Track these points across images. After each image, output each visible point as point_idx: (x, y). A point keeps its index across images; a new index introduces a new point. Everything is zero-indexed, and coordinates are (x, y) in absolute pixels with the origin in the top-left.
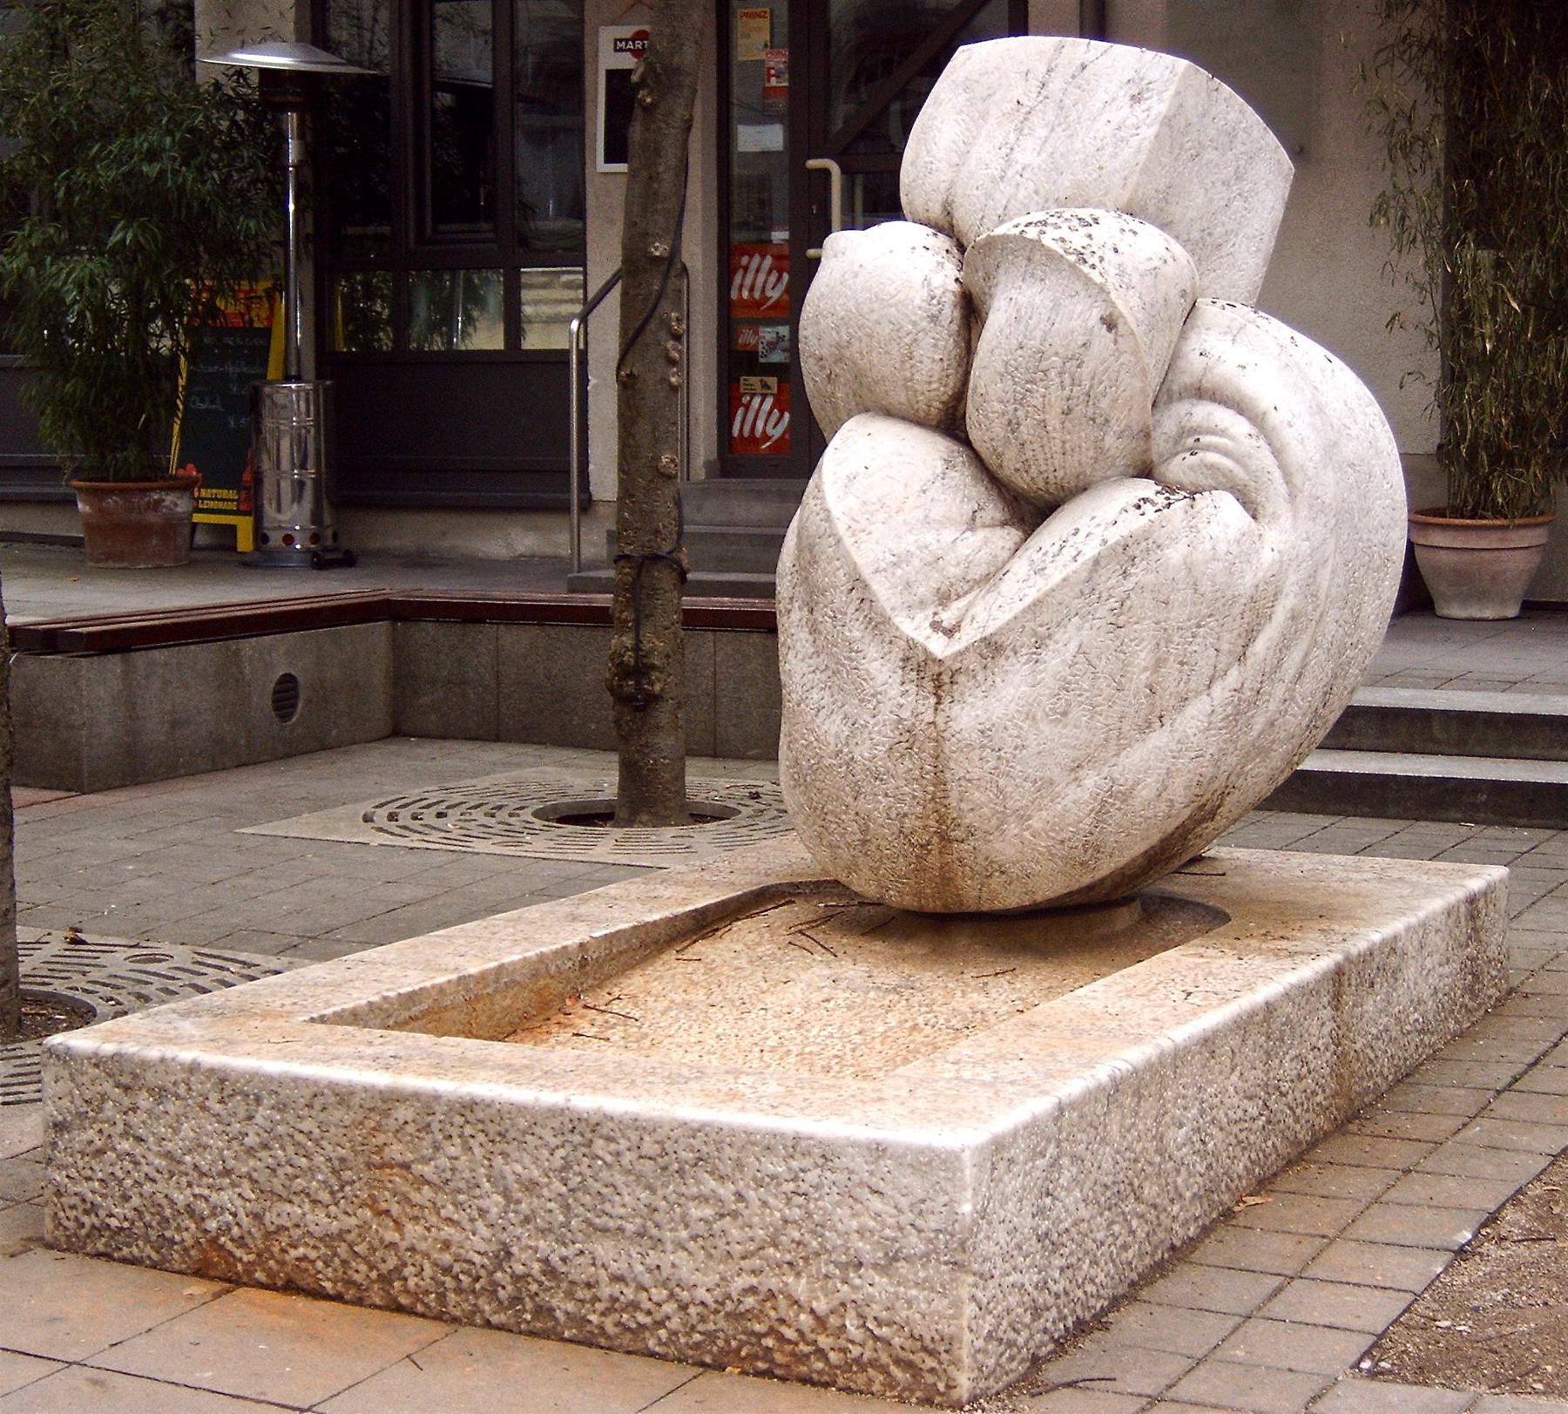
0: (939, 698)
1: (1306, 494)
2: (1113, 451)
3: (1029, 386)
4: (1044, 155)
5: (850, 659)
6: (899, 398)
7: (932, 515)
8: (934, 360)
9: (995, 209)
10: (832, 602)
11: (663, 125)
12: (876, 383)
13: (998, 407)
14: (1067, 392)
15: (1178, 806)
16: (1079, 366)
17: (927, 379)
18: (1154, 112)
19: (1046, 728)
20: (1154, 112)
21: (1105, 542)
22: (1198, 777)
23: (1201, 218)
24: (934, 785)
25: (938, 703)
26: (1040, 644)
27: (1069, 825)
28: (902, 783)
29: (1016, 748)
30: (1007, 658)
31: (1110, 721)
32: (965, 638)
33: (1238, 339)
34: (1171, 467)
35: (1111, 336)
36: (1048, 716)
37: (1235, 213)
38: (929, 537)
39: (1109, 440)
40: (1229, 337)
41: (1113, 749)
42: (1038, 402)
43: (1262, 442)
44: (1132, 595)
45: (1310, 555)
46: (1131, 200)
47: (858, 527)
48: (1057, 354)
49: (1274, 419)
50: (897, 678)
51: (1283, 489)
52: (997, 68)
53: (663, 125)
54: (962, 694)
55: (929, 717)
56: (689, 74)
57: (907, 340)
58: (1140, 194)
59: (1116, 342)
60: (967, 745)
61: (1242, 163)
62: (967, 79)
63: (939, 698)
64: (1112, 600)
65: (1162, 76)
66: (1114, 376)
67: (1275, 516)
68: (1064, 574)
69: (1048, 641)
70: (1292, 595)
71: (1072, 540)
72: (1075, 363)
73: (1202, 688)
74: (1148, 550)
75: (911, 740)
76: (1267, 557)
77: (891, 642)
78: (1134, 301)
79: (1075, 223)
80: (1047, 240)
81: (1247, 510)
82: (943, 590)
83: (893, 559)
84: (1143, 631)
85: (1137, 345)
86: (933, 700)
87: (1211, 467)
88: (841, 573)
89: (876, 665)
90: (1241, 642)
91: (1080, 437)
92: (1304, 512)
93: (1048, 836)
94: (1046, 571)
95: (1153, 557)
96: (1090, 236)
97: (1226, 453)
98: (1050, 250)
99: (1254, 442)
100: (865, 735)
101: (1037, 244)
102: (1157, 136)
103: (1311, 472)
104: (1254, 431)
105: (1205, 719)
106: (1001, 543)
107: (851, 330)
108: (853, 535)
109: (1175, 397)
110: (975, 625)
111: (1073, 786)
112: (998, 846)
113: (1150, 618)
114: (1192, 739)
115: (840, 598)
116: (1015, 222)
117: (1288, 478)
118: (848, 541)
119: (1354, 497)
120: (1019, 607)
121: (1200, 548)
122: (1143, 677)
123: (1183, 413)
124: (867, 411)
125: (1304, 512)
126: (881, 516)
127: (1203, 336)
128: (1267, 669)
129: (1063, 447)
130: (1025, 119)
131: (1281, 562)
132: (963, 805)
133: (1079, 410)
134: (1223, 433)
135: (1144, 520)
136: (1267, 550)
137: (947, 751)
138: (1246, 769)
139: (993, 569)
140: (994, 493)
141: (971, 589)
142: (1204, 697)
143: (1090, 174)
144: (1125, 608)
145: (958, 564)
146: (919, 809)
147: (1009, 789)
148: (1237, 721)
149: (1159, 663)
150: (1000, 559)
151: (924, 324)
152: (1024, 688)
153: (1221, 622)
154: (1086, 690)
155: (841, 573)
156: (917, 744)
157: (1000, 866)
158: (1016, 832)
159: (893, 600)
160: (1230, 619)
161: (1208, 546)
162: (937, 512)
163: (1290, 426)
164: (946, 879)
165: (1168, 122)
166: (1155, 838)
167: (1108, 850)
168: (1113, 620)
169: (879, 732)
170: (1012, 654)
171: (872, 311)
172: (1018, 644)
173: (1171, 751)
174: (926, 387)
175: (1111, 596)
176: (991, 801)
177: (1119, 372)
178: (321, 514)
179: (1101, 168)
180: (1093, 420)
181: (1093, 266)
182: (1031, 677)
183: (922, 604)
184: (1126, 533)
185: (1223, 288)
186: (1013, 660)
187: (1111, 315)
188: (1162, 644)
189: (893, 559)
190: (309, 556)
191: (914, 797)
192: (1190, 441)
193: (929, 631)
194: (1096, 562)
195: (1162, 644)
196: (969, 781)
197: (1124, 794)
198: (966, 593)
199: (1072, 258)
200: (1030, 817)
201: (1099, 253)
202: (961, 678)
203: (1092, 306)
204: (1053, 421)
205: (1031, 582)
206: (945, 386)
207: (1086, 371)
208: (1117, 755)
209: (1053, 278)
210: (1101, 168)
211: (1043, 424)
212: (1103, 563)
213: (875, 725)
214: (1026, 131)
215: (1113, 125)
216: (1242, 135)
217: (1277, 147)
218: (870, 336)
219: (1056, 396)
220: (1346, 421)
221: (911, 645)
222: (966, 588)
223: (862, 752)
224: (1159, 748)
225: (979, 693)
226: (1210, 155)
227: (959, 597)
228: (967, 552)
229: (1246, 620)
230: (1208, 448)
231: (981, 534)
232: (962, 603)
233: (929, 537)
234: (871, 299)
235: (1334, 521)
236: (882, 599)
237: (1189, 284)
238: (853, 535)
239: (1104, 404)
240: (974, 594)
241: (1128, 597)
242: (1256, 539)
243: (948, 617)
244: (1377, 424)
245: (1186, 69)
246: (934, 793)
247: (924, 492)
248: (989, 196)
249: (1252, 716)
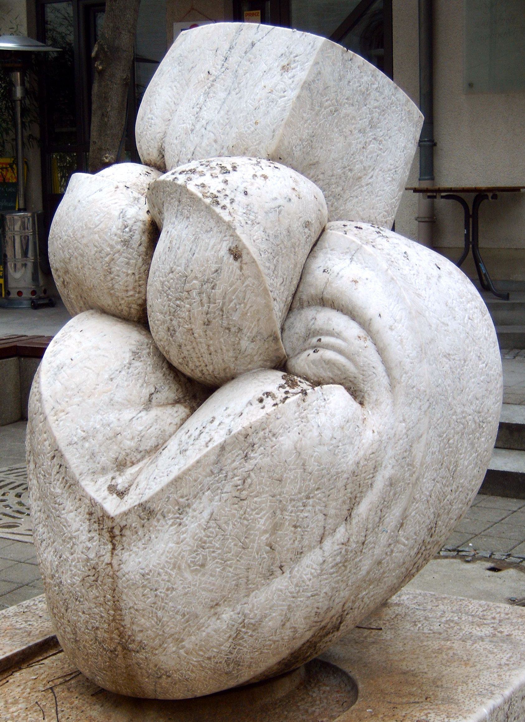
0: (114, 545)
1: (404, 384)
2: (249, 351)
3: (178, 302)
4: (222, 112)
5: (54, 508)
6: (107, 302)
7: (116, 399)
8: (127, 275)
9: (186, 155)
10: (43, 465)
11: (109, 83)
12: (91, 290)
13: (160, 317)
14: (206, 308)
15: (300, 631)
16: (213, 288)
17: (125, 288)
18: (297, 79)
19: (188, 576)
20: (297, 79)
21: (230, 431)
22: (316, 610)
23: (342, 159)
24: (115, 610)
25: (114, 549)
26: (182, 509)
27: (212, 647)
28: (93, 606)
29: (168, 590)
30: (158, 520)
31: (238, 571)
32: (130, 501)
33: (355, 258)
34: (299, 361)
35: (237, 264)
36: (190, 566)
37: (371, 152)
38: (112, 417)
39: (245, 344)
40: (348, 257)
41: (243, 592)
42: (185, 315)
43: (369, 343)
44: (252, 474)
45: (406, 434)
46: (278, 148)
47: (60, 407)
48: (196, 278)
49: (378, 324)
50: (86, 526)
51: (385, 381)
52: (199, 47)
53: (109, 83)
54: (129, 544)
55: (107, 559)
56: (125, 51)
57: (107, 259)
58: (286, 143)
59: (241, 269)
60: (134, 584)
61: (376, 115)
62: (181, 56)
63: (114, 545)
64: (236, 478)
65: (305, 50)
66: (241, 295)
67: (377, 403)
68: (198, 457)
69: (187, 509)
70: (390, 467)
71: (209, 427)
72: (210, 285)
73: (313, 544)
74: (265, 438)
75: (96, 575)
76: (368, 437)
77: (80, 500)
78: (258, 233)
79: (217, 171)
80: (191, 187)
81: (355, 398)
82: (120, 459)
83: (83, 434)
84: (261, 503)
85: (259, 271)
86: (110, 546)
87: (329, 363)
88: (47, 443)
89: (72, 515)
90: (346, 507)
91: (220, 342)
92: (401, 399)
93: (198, 655)
94: (188, 453)
95: (269, 443)
96: (226, 182)
97: (340, 351)
98: (192, 194)
99: (362, 343)
100: (67, 567)
101: (183, 189)
102: (298, 97)
103: (408, 367)
104: (362, 333)
105: (318, 568)
106: (169, 421)
107: (70, 251)
108: (56, 414)
109: (305, 304)
110: (138, 491)
111: (214, 619)
112: (162, 658)
113: (267, 492)
114: (308, 583)
115: (47, 463)
116: (173, 171)
117: (388, 371)
118: (51, 419)
119: (449, 381)
120: (166, 480)
121: (309, 435)
122: (264, 538)
123: (310, 317)
124: (92, 309)
125: (401, 399)
126: (76, 400)
127: (329, 256)
128: (370, 526)
129: (208, 349)
130: (212, 85)
131: (381, 441)
132: (134, 627)
133: (216, 322)
134: (338, 335)
135: (263, 413)
136: (369, 433)
137: (120, 586)
138: (360, 596)
139: (161, 442)
140: (170, 378)
141: (143, 458)
142: (317, 550)
143: (249, 128)
144: (247, 485)
145: (133, 438)
146: (106, 626)
147: (165, 619)
148: (345, 567)
149: (276, 528)
150: (167, 433)
151: (119, 247)
152: (171, 545)
153: (328, 493)
154: (218, 549)
155: (47, 443)
156: (100, 579)
157: (166, 672)
158: (174, 649)
159: (82, 467)
160: (334, 491)
161: (315, 433)
162: (119, 396)
163: (391, 329)
164: (131, 677)
165: (307, 86)
166: (285, 653)
167: (246, 664)
168: (237, 494)
169: (75, 566)
170: (161, 517)
171: (83, 237)
172: (165, 510)
173: (291, 593)
174: (124, 294)
175: (235, 475)
176: (153, 626)
177: (245, 292)
178: (37, 277)
179: (256, 123)
180: (229, 329)
181: (224, 207)
182: (175, 536)
183: (104, 471)
184: (246, 424)
185: (364, 210)
186: (162, 521)
187: (237, 247)
188: (278, 512)
189: (83, 434)
190: (30, 302)
191: (102, 617)
192: (314, 340)
193: (107, 492)
194: (222, 448)
195: (278, 512)
196: (136, 610)
197: (254, 625)
198: (139, 461)
199: (208, 201)
200: (183, 640)
201: (231, 196)
202: (127, 532)
203: (222, 240)
204: (198, 331)
205: (177, 460)
206: (139, 293)
207: (218, 291)
208: (248, 596)
209: (195, 216)
210: (256, 123)
211: (191, 331)
212: (228, 448)
214: (211, 95)
215: (267, 90)
216: (374, 94)
217: (408, 101)
218: (82, 256)
219: (197, 310)
220: (445, 320)
221: (93, 504)
222: (139, 456)
223: (66, 579)
224: (281, 591)
225: (140, 544)
226: (347, 110)
227: (133, 464)
228: (140, 428)
229: (349, 490)
230: (328, 347)
231: (154, 412)
232: (133, 470)
233: (112, 417)
234: (82, 227)
235: (428, 404)
236: (73, 466)
237: (314, 216)
238: (56, 414)
239: (235, 317)
240: (145, 461)
241: (249, 476)
242: (359, 423)
243: (121, 482)
244: (477, 316)
245: (324, 44)
246: (114, 616)
247: (112, 380)
248: (183, 144)
249: (360, 561)
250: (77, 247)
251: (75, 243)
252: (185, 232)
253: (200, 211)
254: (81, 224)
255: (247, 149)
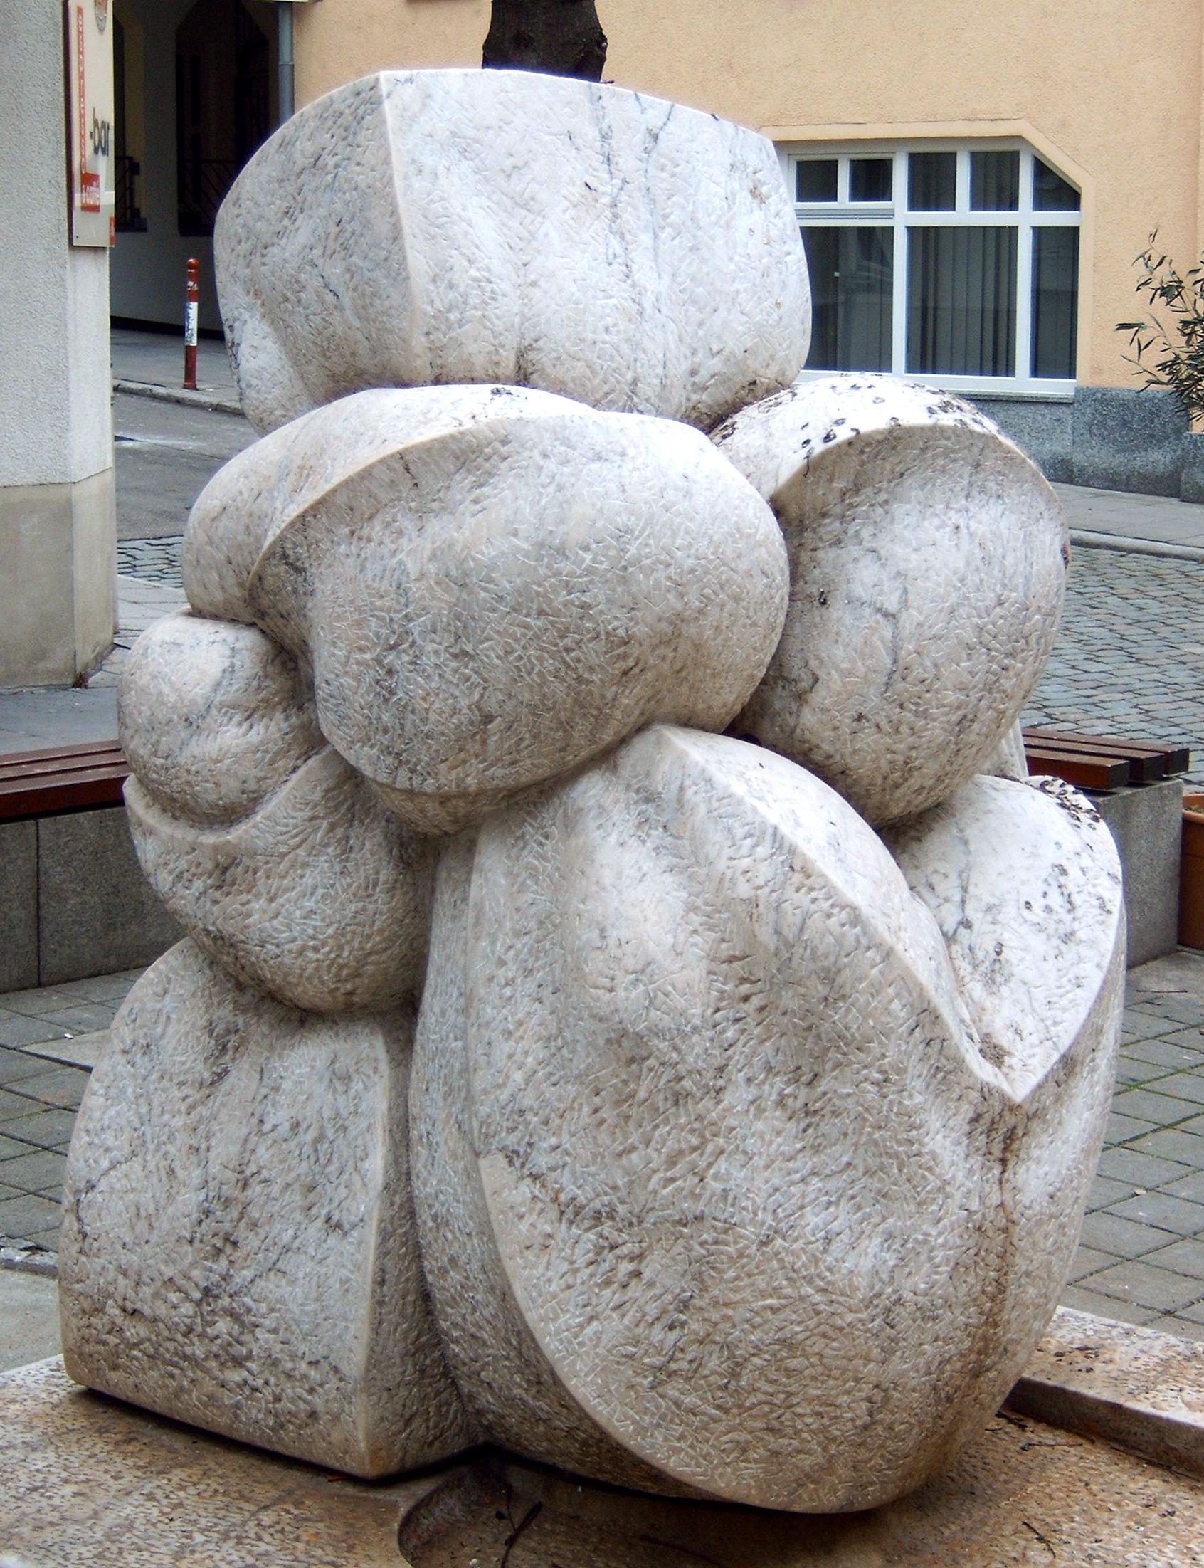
50: (961, 1150)
88: (896, 1005)
155: (896, 1005)
171: (739, 556)
209: (1013, 492)
213: (940, 1234)
250: (727, 581)
251: (721, 573)
252: (1003, 525)
253: (1021, 481)
254: (726, 529)
255: (772, 357)
